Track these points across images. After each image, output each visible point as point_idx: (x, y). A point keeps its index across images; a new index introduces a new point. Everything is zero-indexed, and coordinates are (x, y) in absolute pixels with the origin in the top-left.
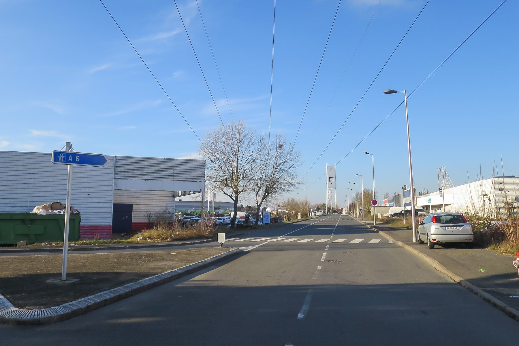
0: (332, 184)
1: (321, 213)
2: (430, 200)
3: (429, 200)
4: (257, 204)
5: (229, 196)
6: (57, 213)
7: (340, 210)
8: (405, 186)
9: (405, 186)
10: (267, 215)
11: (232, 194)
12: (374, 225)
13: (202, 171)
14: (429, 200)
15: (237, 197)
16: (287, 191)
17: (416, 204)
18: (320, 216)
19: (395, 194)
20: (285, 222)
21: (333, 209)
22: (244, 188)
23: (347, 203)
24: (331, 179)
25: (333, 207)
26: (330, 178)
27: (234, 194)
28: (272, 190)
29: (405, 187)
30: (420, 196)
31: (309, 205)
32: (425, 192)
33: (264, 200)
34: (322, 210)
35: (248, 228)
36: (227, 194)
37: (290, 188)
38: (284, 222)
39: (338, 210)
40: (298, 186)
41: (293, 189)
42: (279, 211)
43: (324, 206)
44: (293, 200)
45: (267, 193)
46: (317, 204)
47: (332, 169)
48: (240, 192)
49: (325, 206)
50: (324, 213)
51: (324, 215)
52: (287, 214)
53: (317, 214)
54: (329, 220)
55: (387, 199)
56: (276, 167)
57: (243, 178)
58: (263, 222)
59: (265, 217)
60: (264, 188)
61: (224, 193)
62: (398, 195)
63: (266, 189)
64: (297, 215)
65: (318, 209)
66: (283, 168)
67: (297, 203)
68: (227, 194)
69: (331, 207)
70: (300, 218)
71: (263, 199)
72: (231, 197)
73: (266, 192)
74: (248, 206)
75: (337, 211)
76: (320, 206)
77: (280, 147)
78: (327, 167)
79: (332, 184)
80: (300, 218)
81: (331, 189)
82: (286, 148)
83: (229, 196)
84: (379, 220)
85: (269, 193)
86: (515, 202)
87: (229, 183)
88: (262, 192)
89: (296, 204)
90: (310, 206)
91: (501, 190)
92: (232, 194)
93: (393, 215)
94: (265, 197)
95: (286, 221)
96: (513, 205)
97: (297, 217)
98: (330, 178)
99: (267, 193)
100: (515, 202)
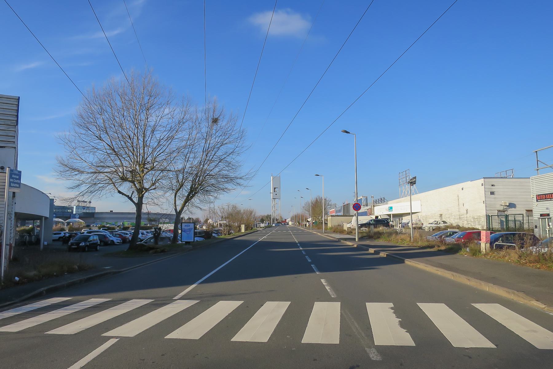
0: (276, 194)
1: (267, 225)
2: (391, 208)
3: (390, 208)
4: (176, 210)
5: (128, 196)
6: (29, 225)
7: (284, 221)
8: (415, 178)
9: (415, 178)
10: (189, 228)
11: (132, 194)
12: (357, 241)
13: (9, 123)
14: (390, 208)
15: (141, 199)
16: (223, 190)
17: (373, 213)
18: (266, 227)
19: (344, 204)
20: (223, 236)
21: (277, 220)
22: (153, 184)
23: (292, 214)
24: (276, 190)
25: (278, 218)
26: (275, 188)
27: (136, 193)
28: (201, 188)
29: (414, 180)
30: (379, 204)
31: (254, 215)
32: (382, 201)
33: (187, 204)
34: (266, 221)
35: (151, 252)
36: (123, 194)
37: (229, 186)
38: (221, 237)
39: (283, 221)
40: (239, 181)
41: (235, 187)
42: (220, 222)
43: (268, 217)
44: (234, 207)
45: (193, 193)
46: (261, 216)
47: (277, 179)
48: (147, 190)
49: (253, 223)
50: (269, 224)
51: (269, 227)
52: (227, 226)
53: (262, 225)
54: (279, 233)
55: (334, 209)
56: (206, 151)
57: (153, 169)
58: (182, 241)
59: (185, 231)
60: (188, 186)
61: (119, 192)
62: (348, 204)
63: (191, 187)
64: (239, 227)
65: (262, 221)
66: (219, 153)
67: (240, 211)
68: (123, 194)
69: (275, 218)
70: (243, 230)
71: (186, 202)
72: (130, 199)
73: (191, 191)
74: (190, 217)
75: (282, 223)
76: (265, 218)
77: (215, 121)
78: (272, 177)
79: (276, 194)
80: (243, 230)
81: (276, 200)
82: (222, 123)
83: (128, 196)
84: (346, 233)
85: (196, 193)
86: (508, 208)
87: (129, 175)
88: (184, 192)
89: (239, 212)
90: (256, 216)
91: (492, 193)
92: (132, 194)
93: (360, 225)
94: (188, 199)
95: (225, 235)
96: (506, 212)
97: (240, 230)
98: (275, 188)
99: (193, 193)
100: (508, 208)
